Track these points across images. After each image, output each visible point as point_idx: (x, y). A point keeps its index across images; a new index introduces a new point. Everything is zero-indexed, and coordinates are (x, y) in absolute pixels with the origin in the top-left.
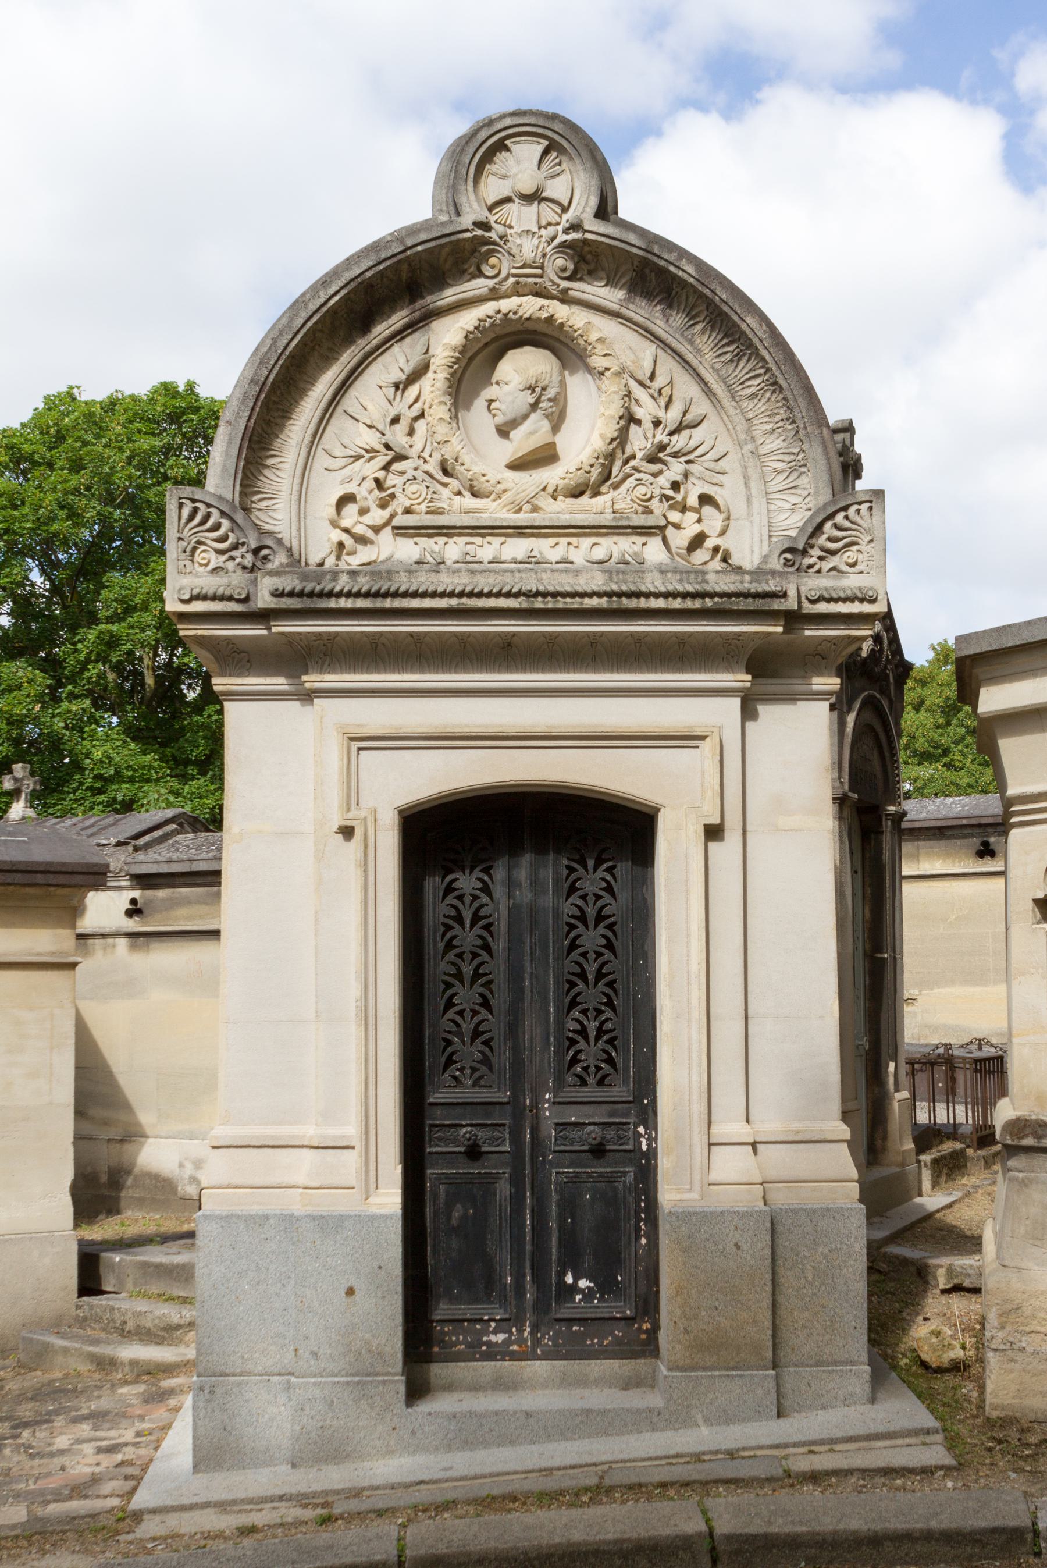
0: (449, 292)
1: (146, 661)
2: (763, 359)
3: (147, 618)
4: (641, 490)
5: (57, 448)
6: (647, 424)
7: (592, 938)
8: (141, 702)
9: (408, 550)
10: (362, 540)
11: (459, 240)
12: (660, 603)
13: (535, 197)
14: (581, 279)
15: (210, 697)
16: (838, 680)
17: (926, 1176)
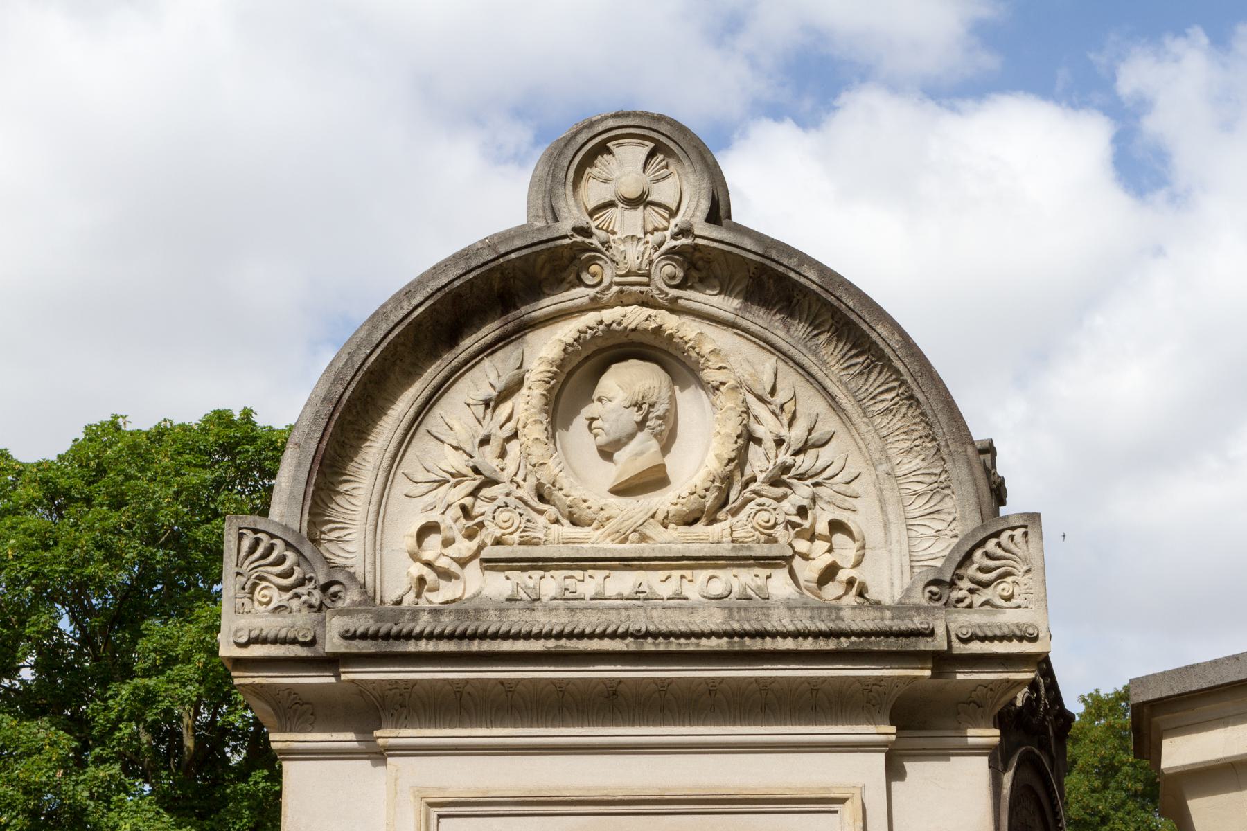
0: (545, 302)
1: (186, 720)
2: (897, 371)
3: (189, 671)
4: (764, 516)
5: (96, 482)
6: (769, 443)
8: (178, 767)
9: (498, 585)
10: (446, 575)
11: (556, 247)
14: (691, 288)
15: (266, 760)
16: (997, 732)
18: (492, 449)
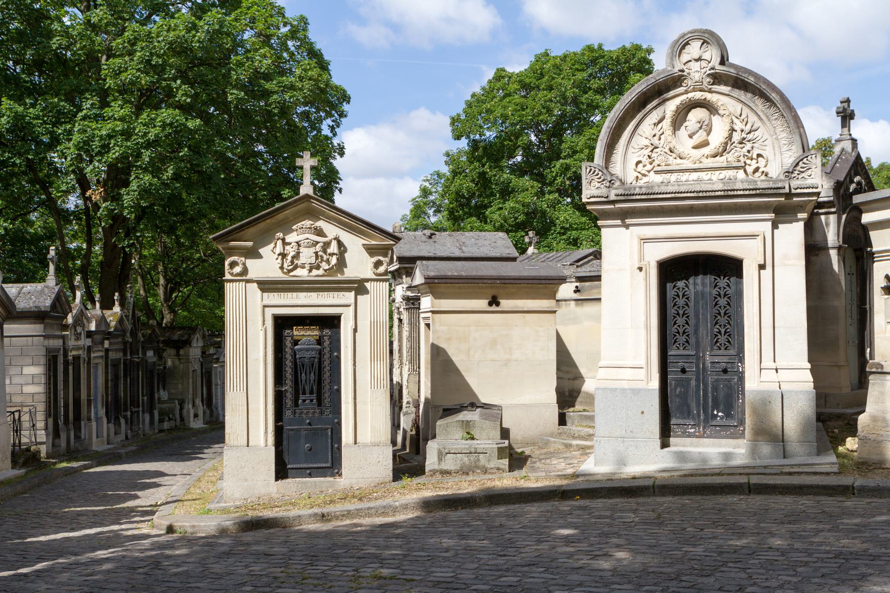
6: (739, 131)
7: (722, 302)
9: (658, 178)
10: (644, 175)
12: (741, 193)
13: (699, 59)
18: (657, 137)
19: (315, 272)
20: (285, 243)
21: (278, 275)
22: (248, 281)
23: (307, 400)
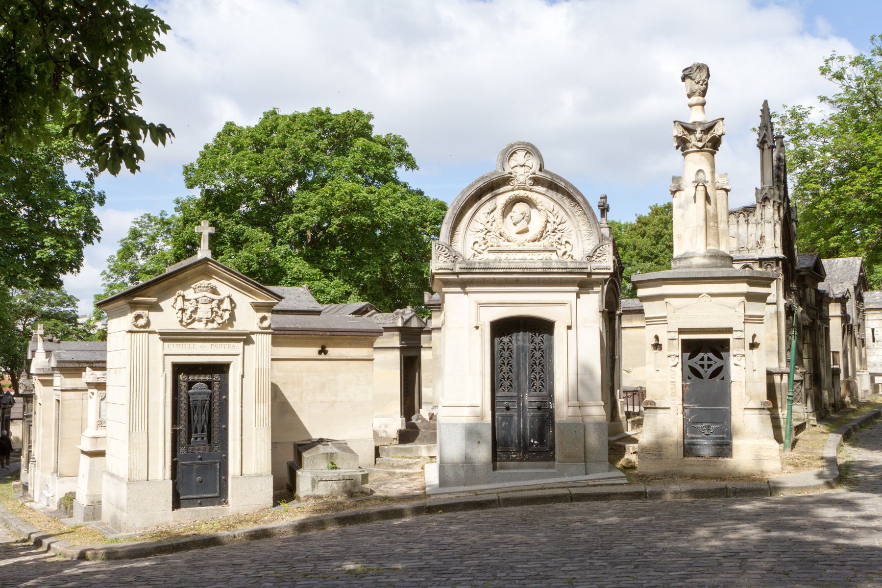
7: (538, 354)
9: (492, 256)
10: (480, 253)
13: (523, 166)
17: (630, 426)
18: (490, 224)
19: (210, 325)
20: (184, 299)
21: (177, 327)
22: (150, 332)
23: (199, 438)
